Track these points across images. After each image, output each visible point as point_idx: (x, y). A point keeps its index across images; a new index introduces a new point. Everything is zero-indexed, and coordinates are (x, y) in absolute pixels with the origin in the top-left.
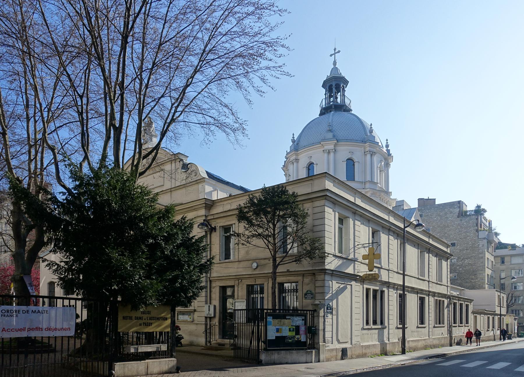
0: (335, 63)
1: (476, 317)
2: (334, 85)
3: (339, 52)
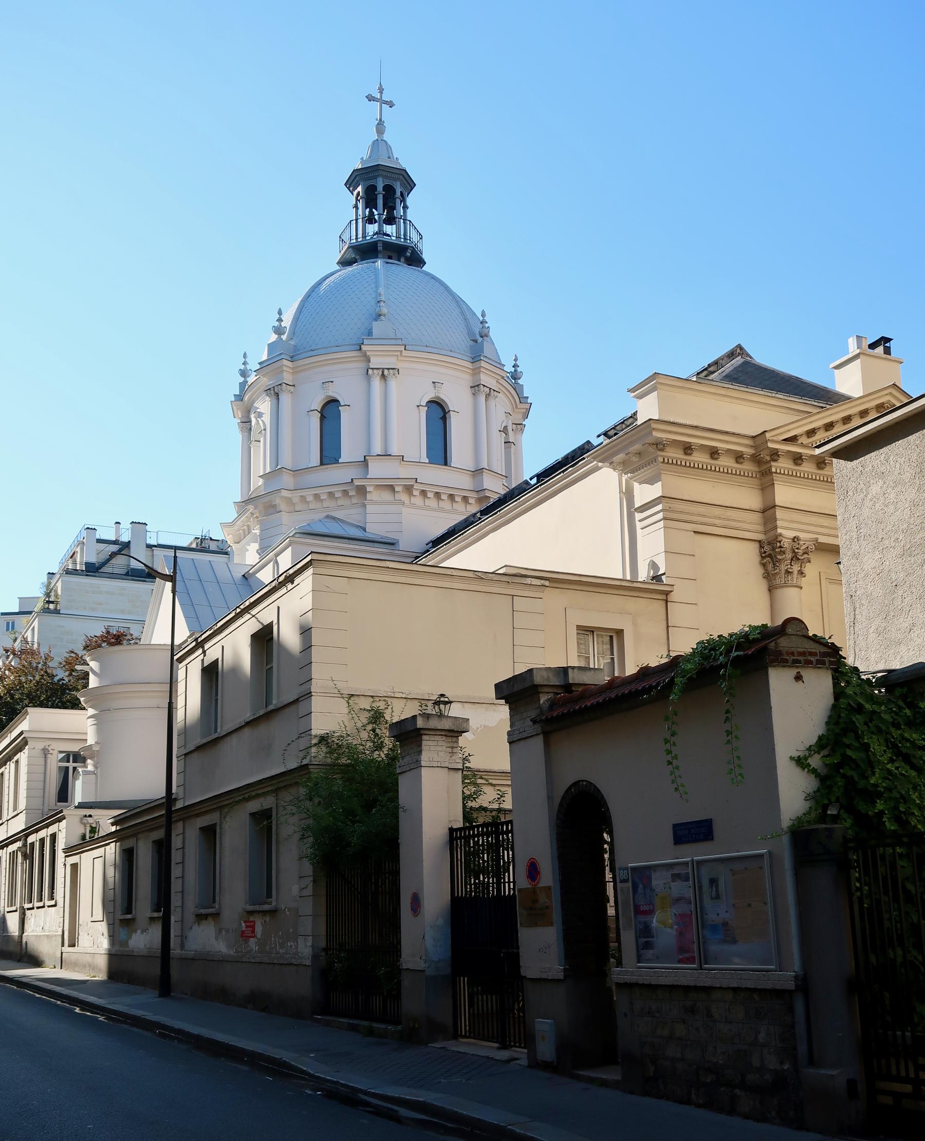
0: (380, 127)
1: (75, 867)
2: (380, 188)
3: (381, 90)
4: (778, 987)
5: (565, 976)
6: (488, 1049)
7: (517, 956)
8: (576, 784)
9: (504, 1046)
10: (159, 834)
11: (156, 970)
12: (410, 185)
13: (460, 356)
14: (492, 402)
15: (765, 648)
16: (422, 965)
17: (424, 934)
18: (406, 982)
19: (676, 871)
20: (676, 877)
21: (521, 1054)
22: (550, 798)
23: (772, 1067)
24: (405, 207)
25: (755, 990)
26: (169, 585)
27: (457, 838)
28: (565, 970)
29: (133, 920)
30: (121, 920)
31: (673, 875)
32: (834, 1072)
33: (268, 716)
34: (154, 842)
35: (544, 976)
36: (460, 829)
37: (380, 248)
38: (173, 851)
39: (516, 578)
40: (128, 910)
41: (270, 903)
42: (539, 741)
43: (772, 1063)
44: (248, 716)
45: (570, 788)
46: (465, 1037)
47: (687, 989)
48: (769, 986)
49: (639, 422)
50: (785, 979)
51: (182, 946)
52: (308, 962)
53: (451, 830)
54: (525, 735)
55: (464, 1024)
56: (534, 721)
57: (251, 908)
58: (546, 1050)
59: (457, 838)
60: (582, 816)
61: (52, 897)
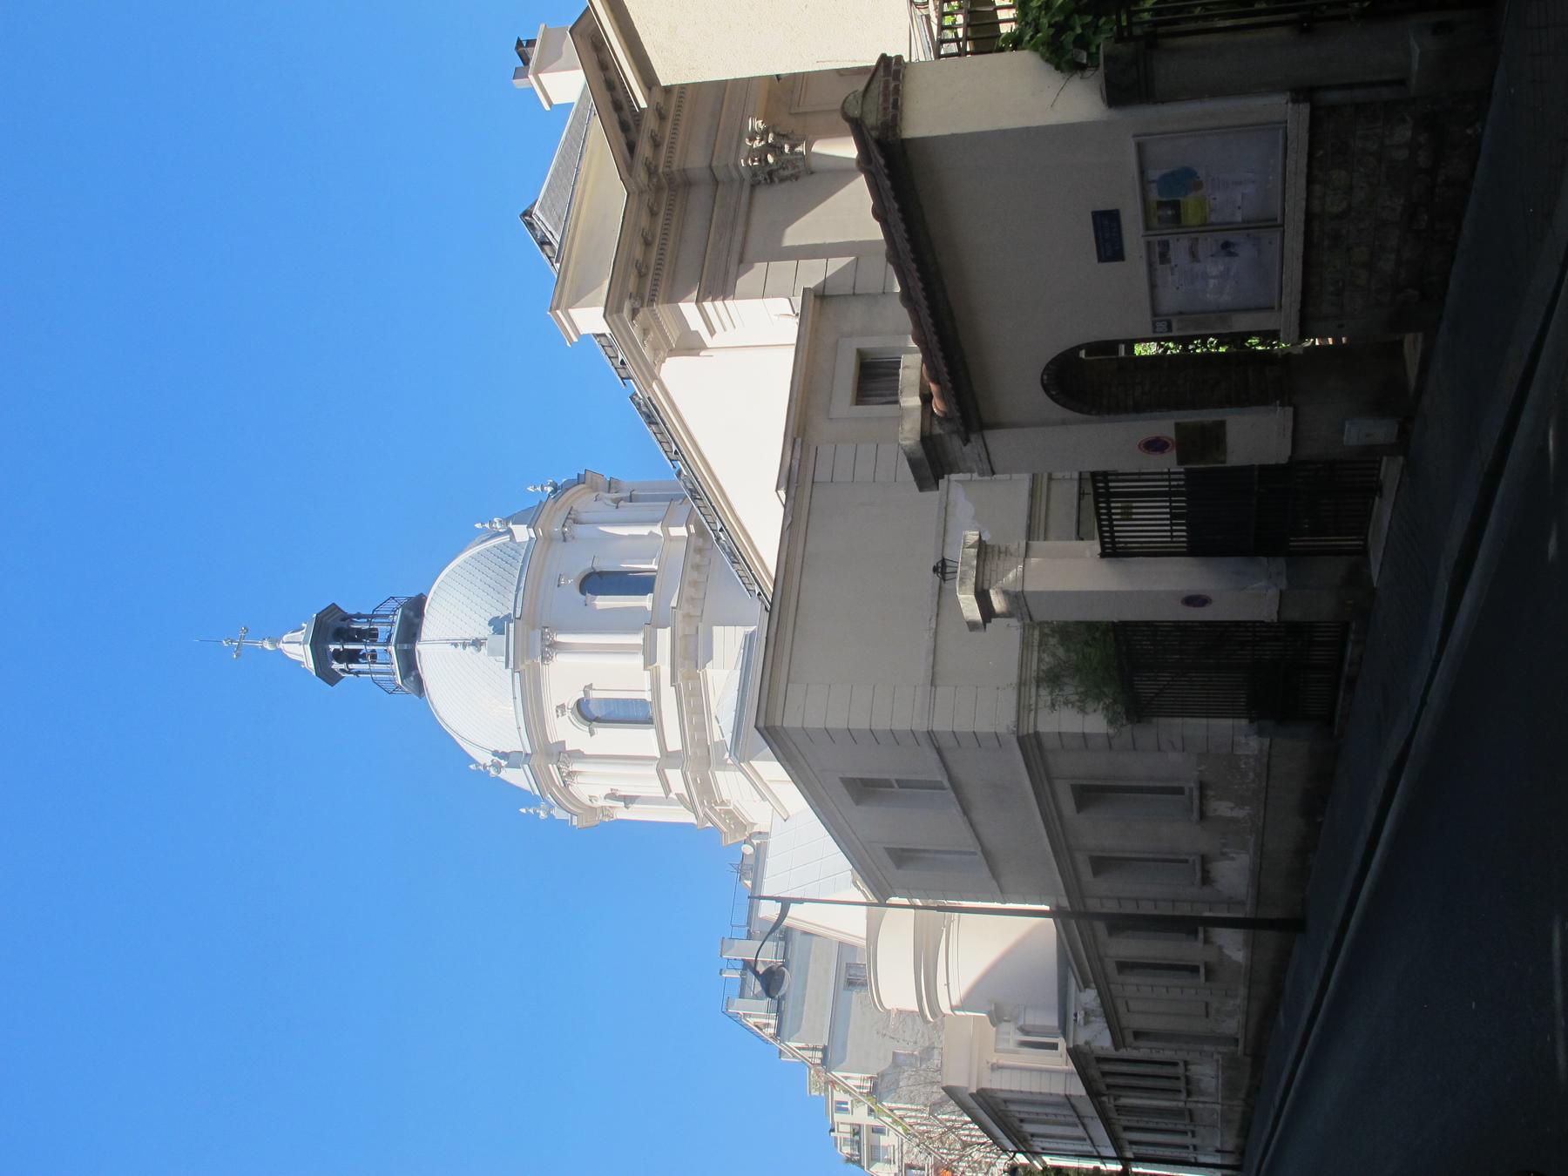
1: (1138, 1035)
4: (1306, 125)
5: (1290, 405)
6: (1384, 512)
7: (1264, 469)
8: (1046, 388)
9: (1378, 489)
10: (1100, 926)
11: (1269, 938)
12: (334, 608)
13: (738, 238)
14: (584, 517)
15: (878, 142)
16: (1273, 593)
17: (1239, 594)
18: (1294, 615)
19: (1156, 258)
20: (1164, 258)
21: (1390, 471)
22: (1064, 423)
23: (1409, 134)
24: (359, 616)
25: (1311, 156)
26: (794, 910)
27: (1114, 548)
28: (1282, 405)
29: (1206, 965)
30: (1207, 979)
31: (1162, 262)
32: (1417, 51)
33: (956, 786)
34: (1110, 934)
35: (1289, 433)
36: (1103, 544)
37: (405, 647)
38: (1122, 911)
39: (796, 480)
40: (1194, 970)
41: (1191, 790)
42: (988, 434)
43: (1403, 133)
44: (956, 810)
45: (1051, 397)
46: (1366, 540)
47: (1309, 245)
48: (1305, 136)
49: (607, 331)
50: (1297, 117)
51: (1242, 903)
52: (1267, 741)
53: (1103, 555)
54: (984, 455)
55: (1351, 542)
56: (966, 441)
57: (1196, 815)
58: (1380, 431)
59: (1114, 548)
60: (1087, 380)
61: (1175, 1064)
